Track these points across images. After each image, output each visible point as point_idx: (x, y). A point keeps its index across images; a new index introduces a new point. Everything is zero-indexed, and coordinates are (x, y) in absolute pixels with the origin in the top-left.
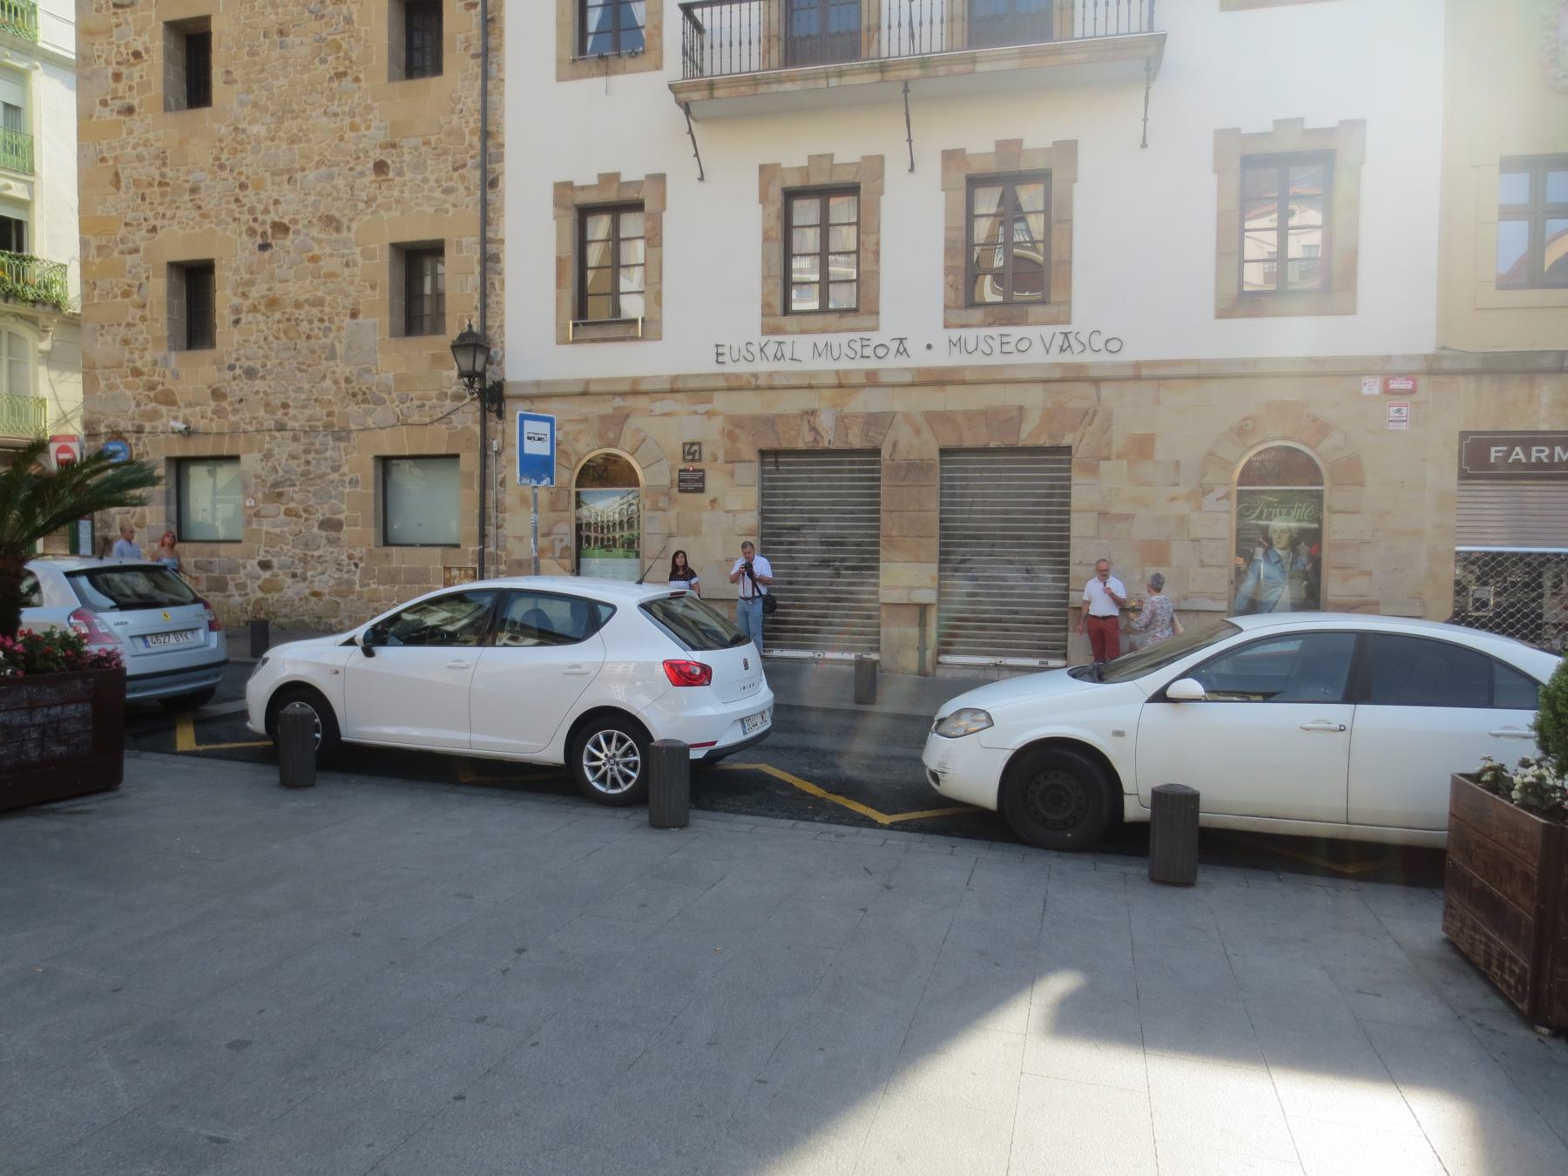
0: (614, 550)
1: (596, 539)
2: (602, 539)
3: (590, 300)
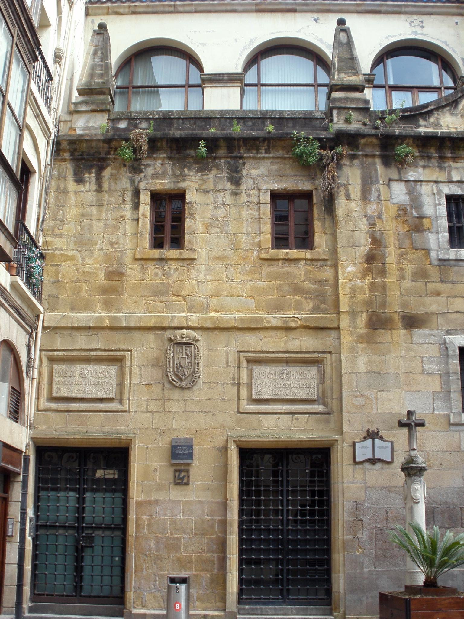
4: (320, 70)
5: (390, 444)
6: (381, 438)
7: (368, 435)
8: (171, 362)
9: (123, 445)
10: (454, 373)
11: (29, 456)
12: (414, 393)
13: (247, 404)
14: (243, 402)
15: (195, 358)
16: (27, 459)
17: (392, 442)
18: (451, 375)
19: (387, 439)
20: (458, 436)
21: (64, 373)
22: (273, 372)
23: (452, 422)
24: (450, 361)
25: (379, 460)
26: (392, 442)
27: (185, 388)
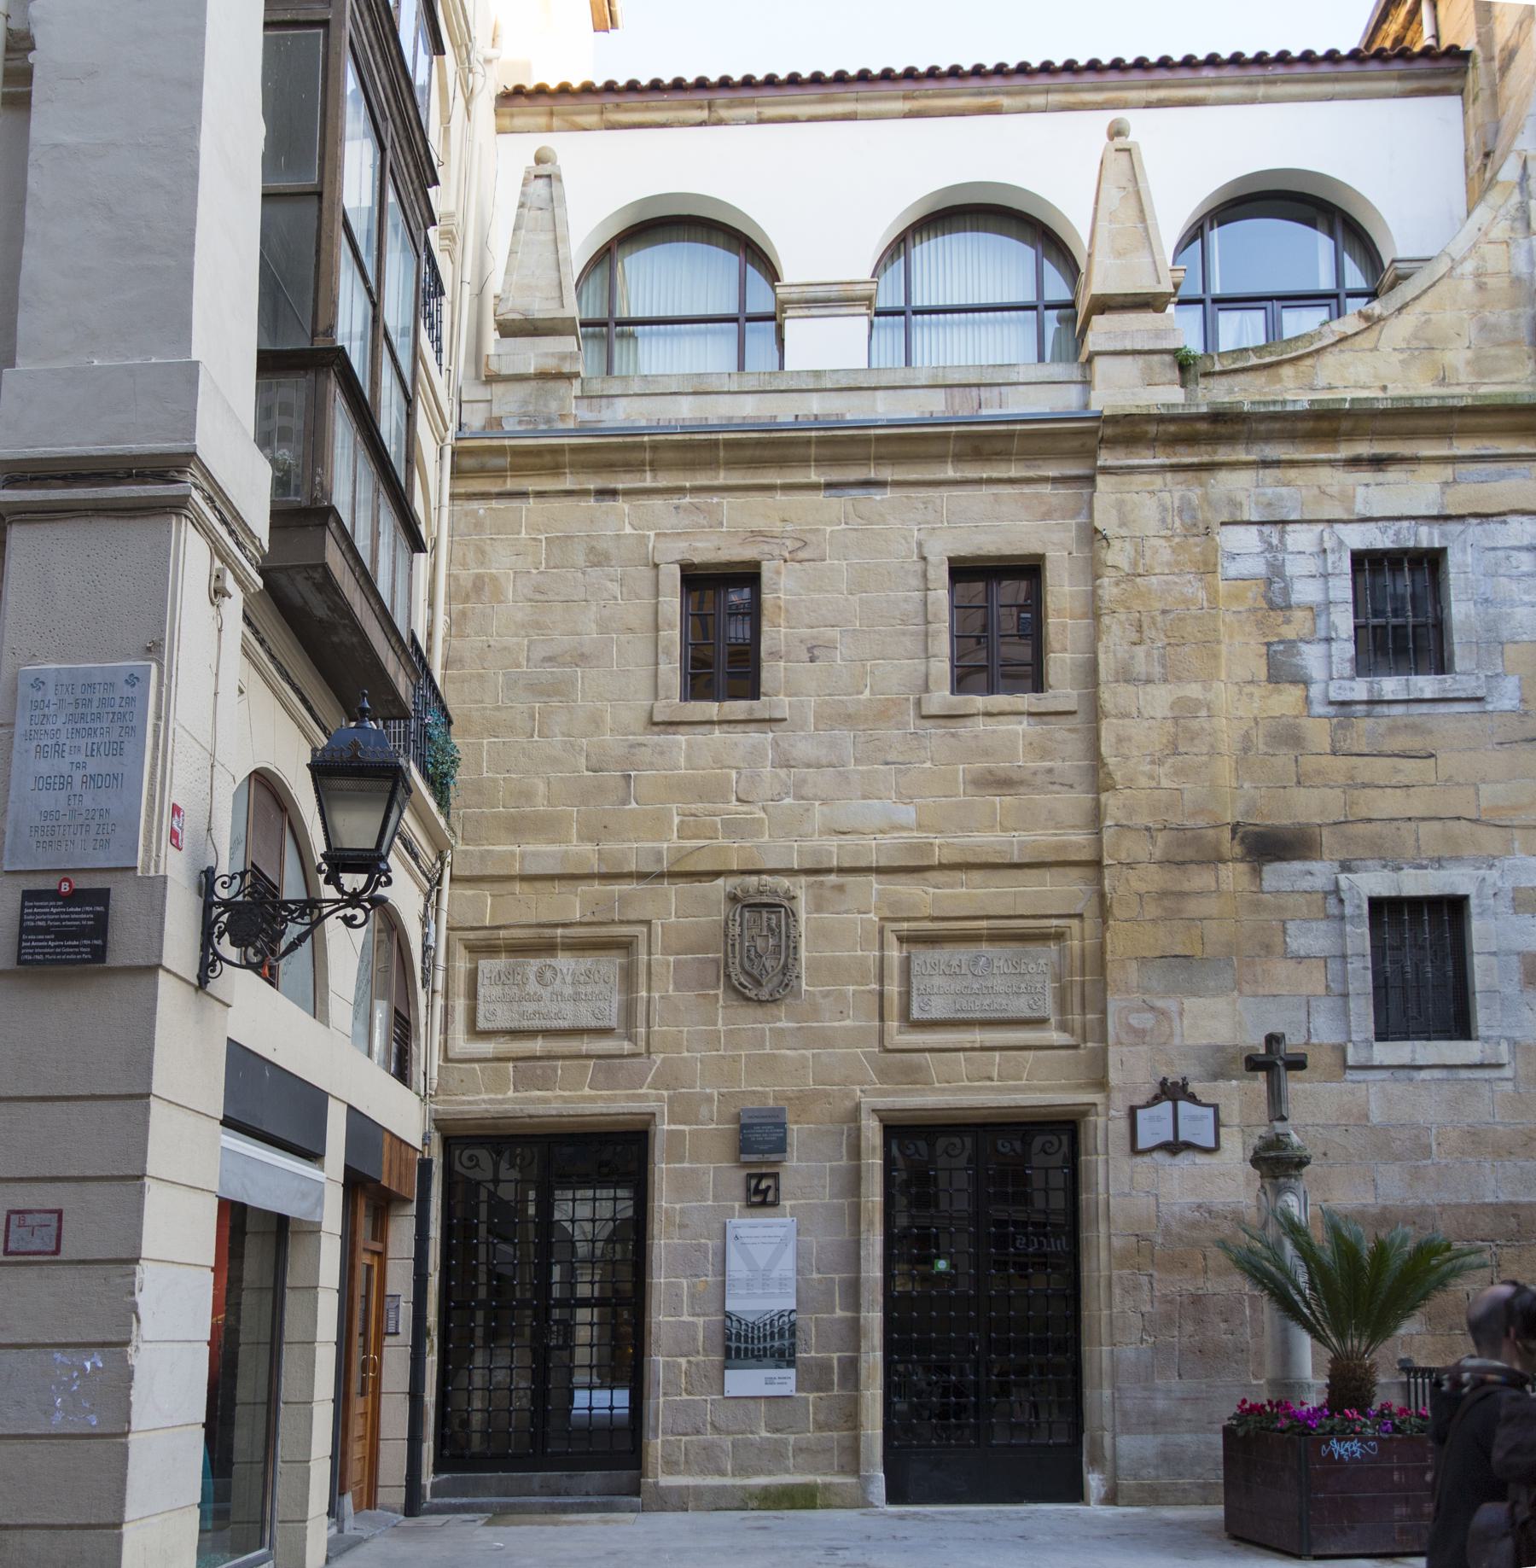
0: (765, 1360)
1: (738, 1349)
2: (753, 1350)
3: (269, 1340)
4: (1051, 271)
5: (1211, 1110)
6: (1192, 1098)
7: (1164, 1092)
8: (737, 946)
9: (639, 1127)
10: (1357, 955)
11: (430, 1161)
12: (1265, 1000)
13: (900, 1033)
14: (893, 1024)
15: (788, 937)
16: (425, 1165)
17: (1216, 1107)
18: (1349, 960)
19: (1204, 1101)
20: (1364, 1093)
21: (503, 978)
22: (954, 963)
23: (1350, 1062)
24: (1348, 928)
25: (1189, 1146)
26: (1216, 1107)
27: (768, 1001)
